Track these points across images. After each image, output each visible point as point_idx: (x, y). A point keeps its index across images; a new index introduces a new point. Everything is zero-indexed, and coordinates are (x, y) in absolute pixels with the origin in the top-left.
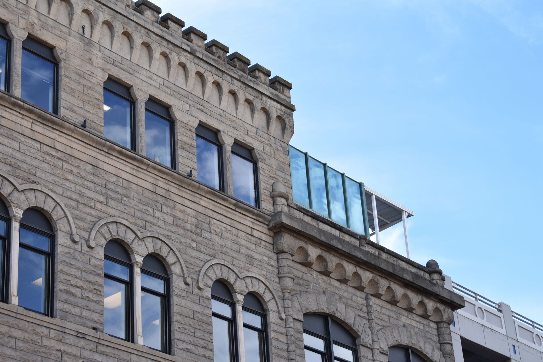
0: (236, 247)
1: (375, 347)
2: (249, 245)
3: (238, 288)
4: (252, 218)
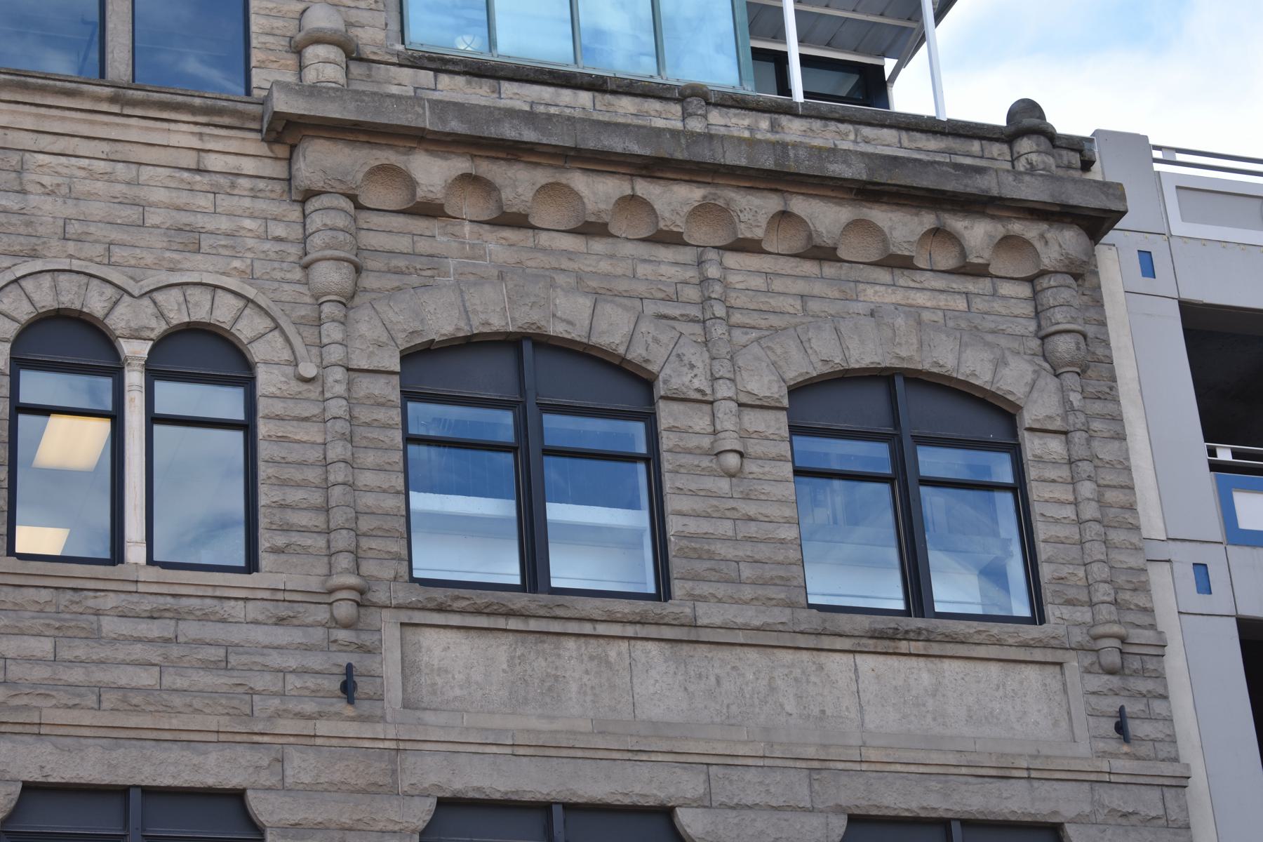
0: (132, 214)
1: (719, 395)
2: (183, 198)
3: (123, 324)
4: (196, 124)
